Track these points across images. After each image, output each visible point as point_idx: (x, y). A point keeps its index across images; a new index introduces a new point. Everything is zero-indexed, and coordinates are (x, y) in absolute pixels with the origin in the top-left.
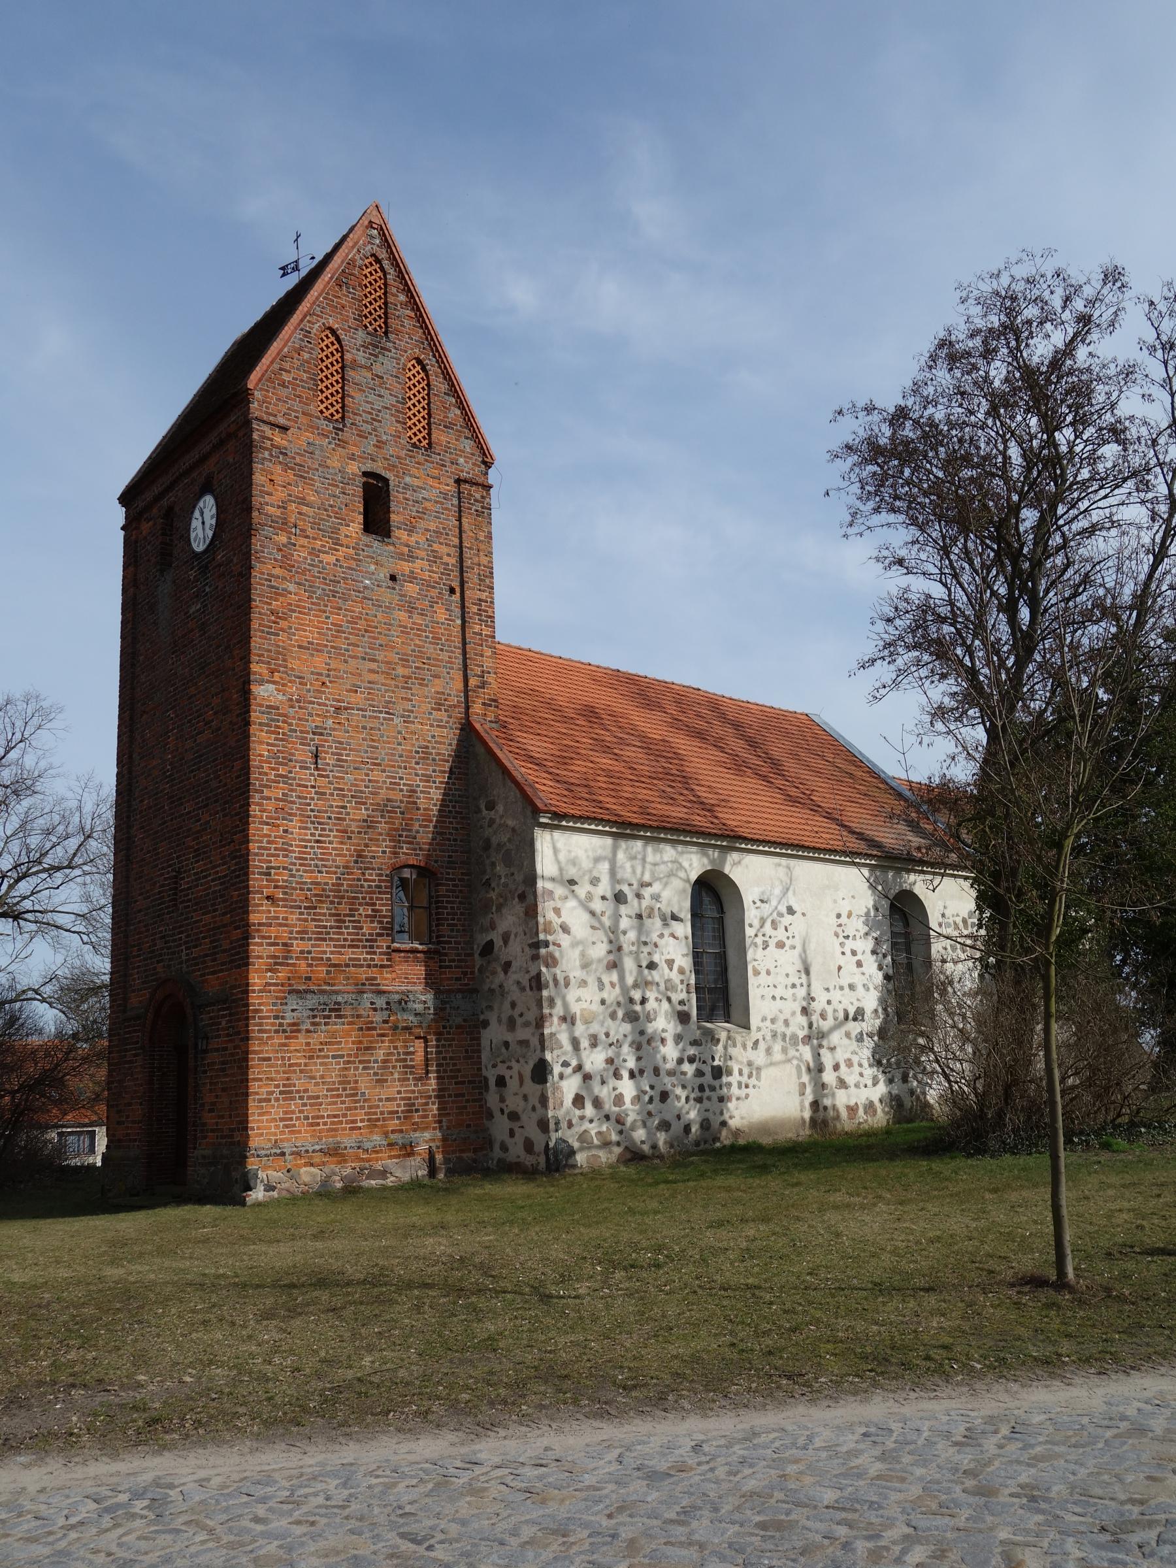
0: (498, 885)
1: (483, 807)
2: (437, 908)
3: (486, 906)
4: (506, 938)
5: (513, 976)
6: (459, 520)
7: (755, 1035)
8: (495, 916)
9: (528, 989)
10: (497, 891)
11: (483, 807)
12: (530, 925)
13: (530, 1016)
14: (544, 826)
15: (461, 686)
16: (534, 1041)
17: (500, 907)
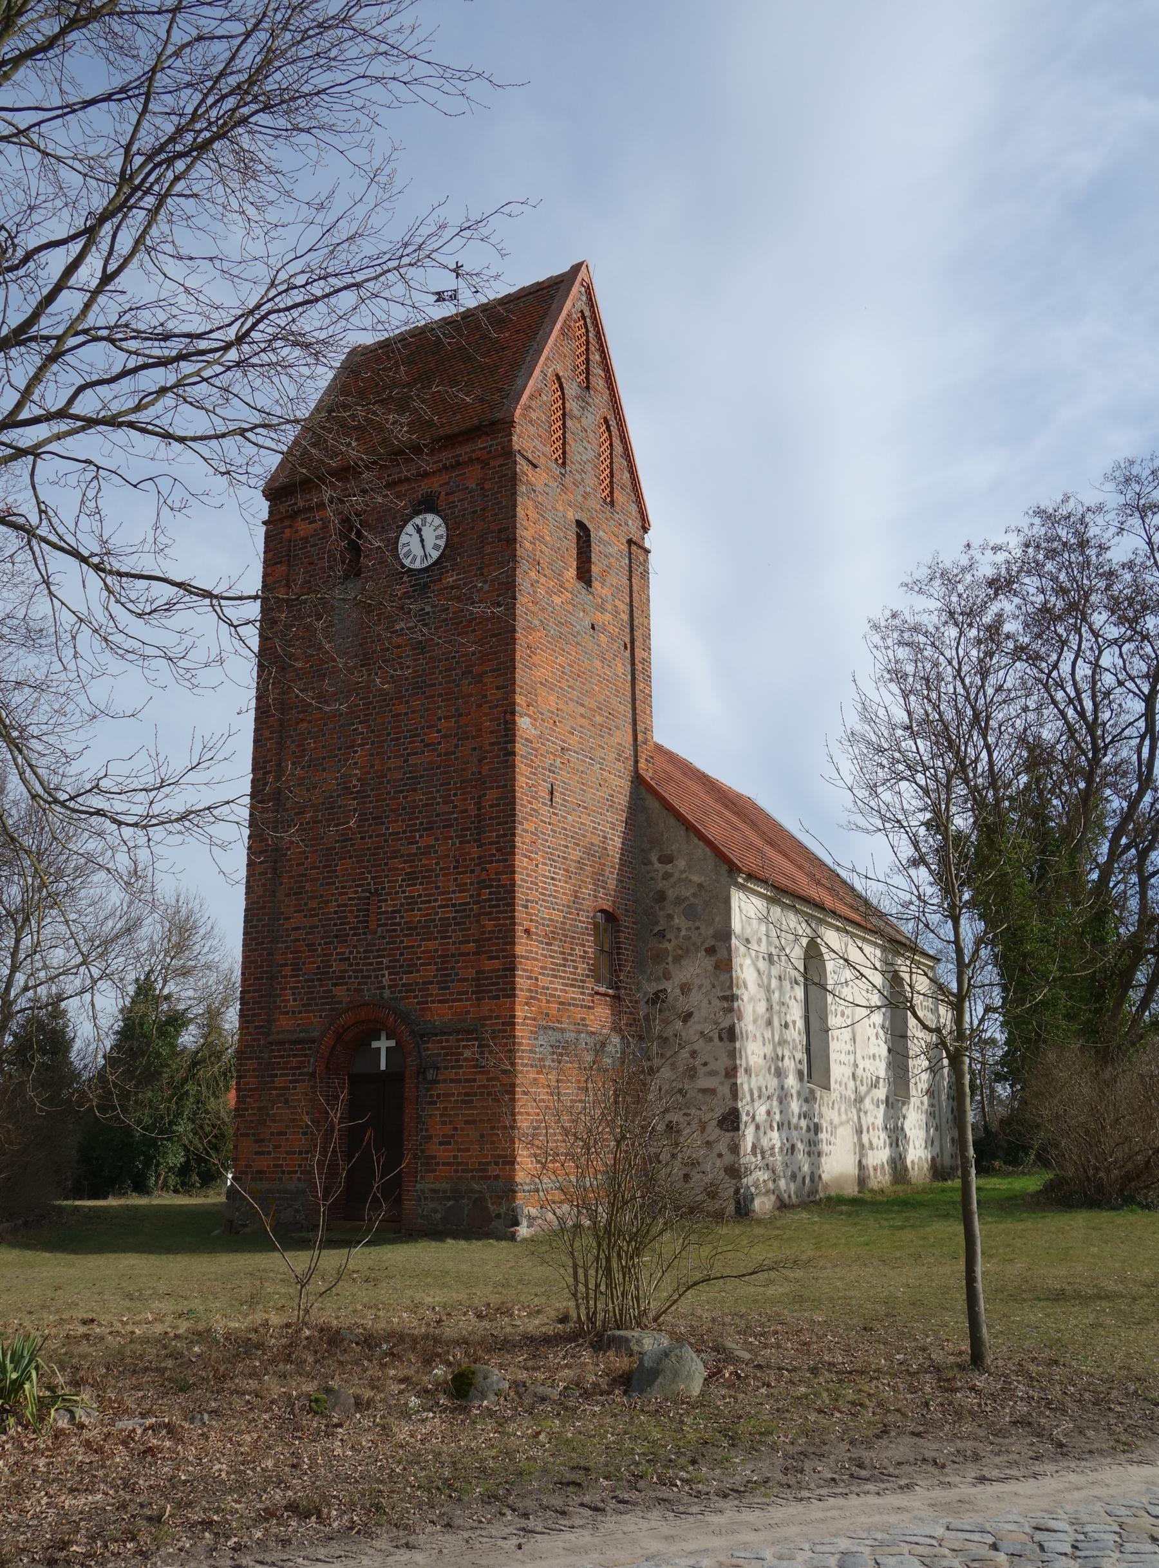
0: (677, 937)
1: (654, 859)
2: (618, 954)
3: (659, 957)
4: (685, 989)
5: (694, 1027)
6: (630, 579)
7: (834, 1095)
8: (671, 967)
9: (716, 1040)
10: (674, 942)
11: (654, 859)
12: (722, 978)
13: (721, 1065)
14: (742, 887)
15: (630, 739)
16: (725, 1090)
17: (677, 959)
